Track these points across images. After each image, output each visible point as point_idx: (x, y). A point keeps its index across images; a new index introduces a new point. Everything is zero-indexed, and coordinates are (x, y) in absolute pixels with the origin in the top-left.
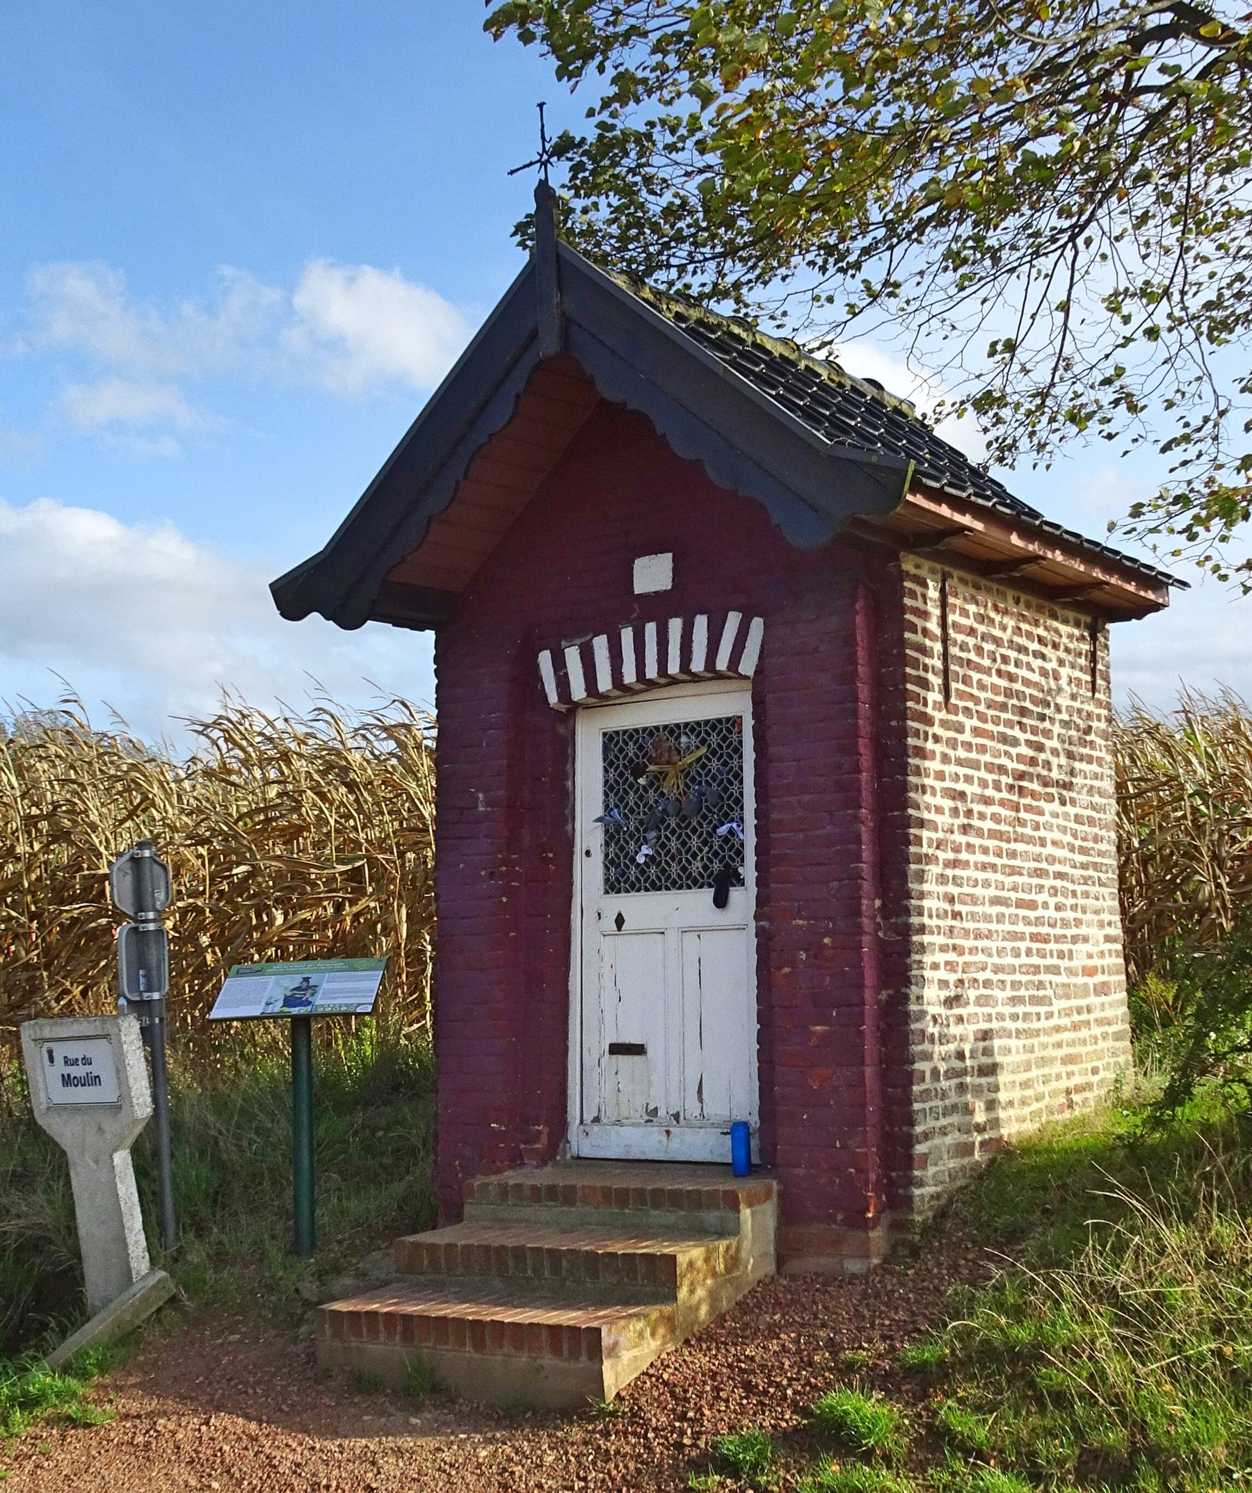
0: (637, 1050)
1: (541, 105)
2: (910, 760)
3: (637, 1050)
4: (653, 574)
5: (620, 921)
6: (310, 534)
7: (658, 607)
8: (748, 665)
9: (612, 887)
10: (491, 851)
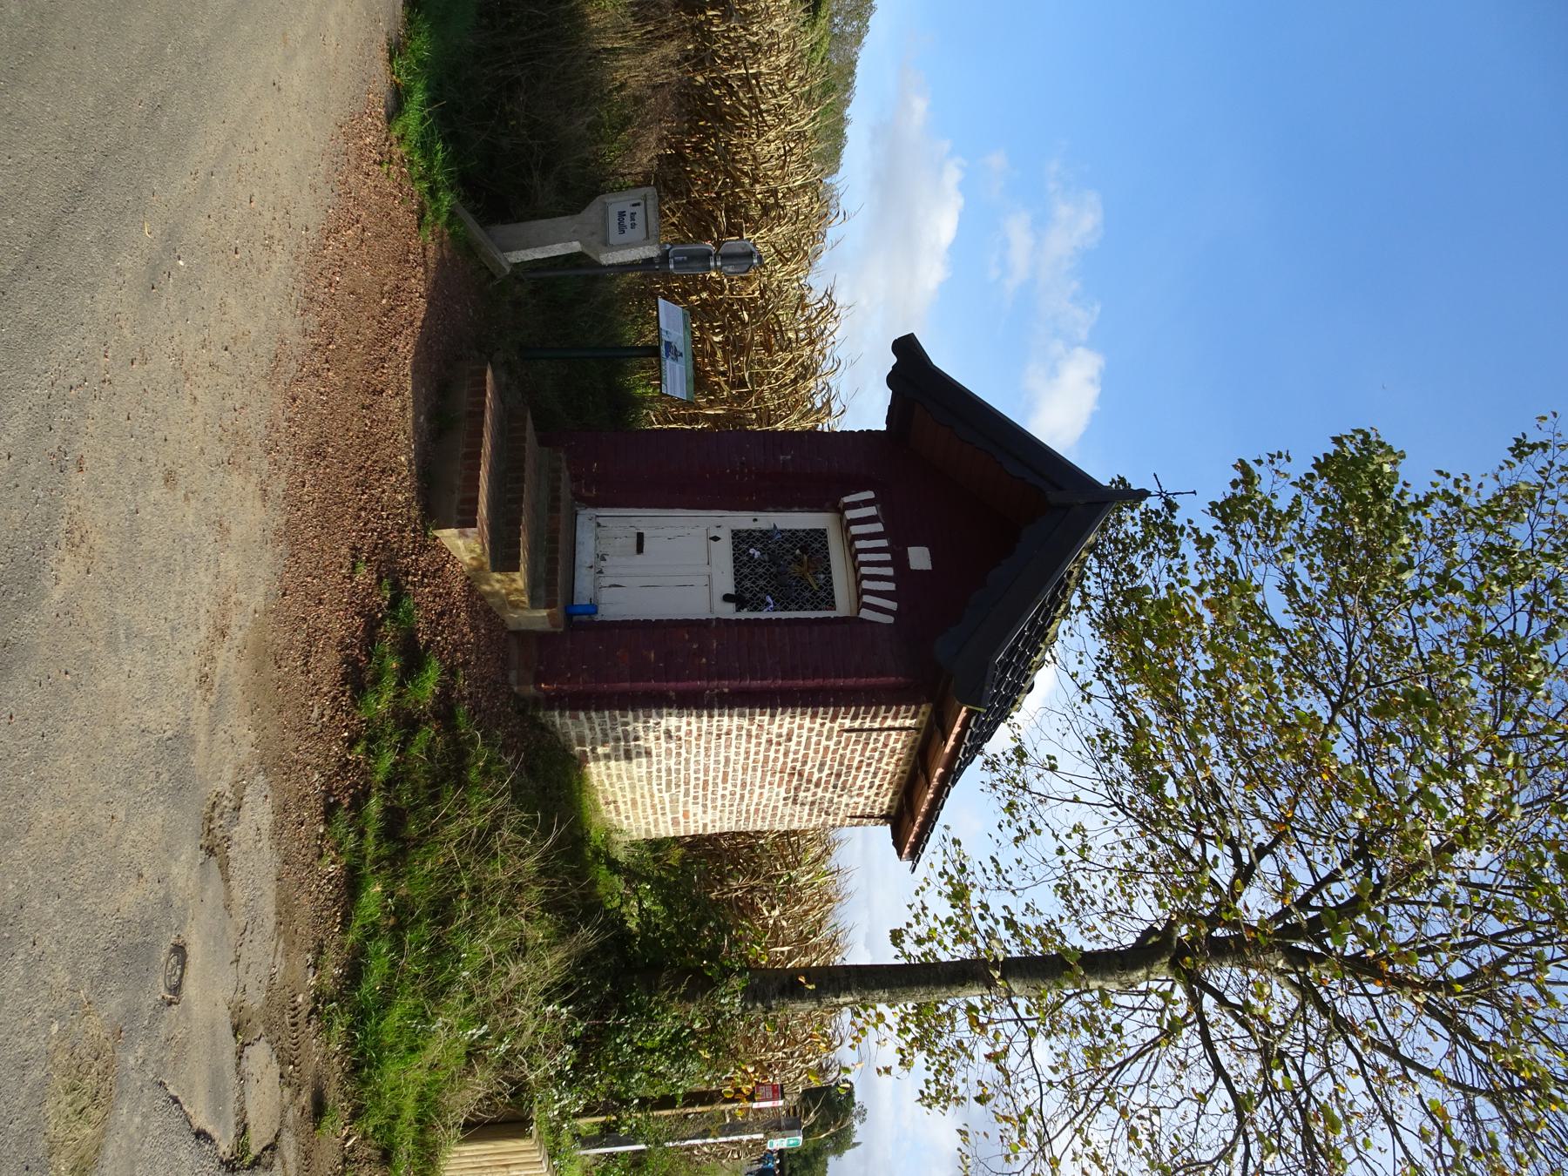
3: (640, 550)
4: (919, 558)
5: (716, 539)
7: (900, 561)
8: (865, 614)
9: (736, 534)
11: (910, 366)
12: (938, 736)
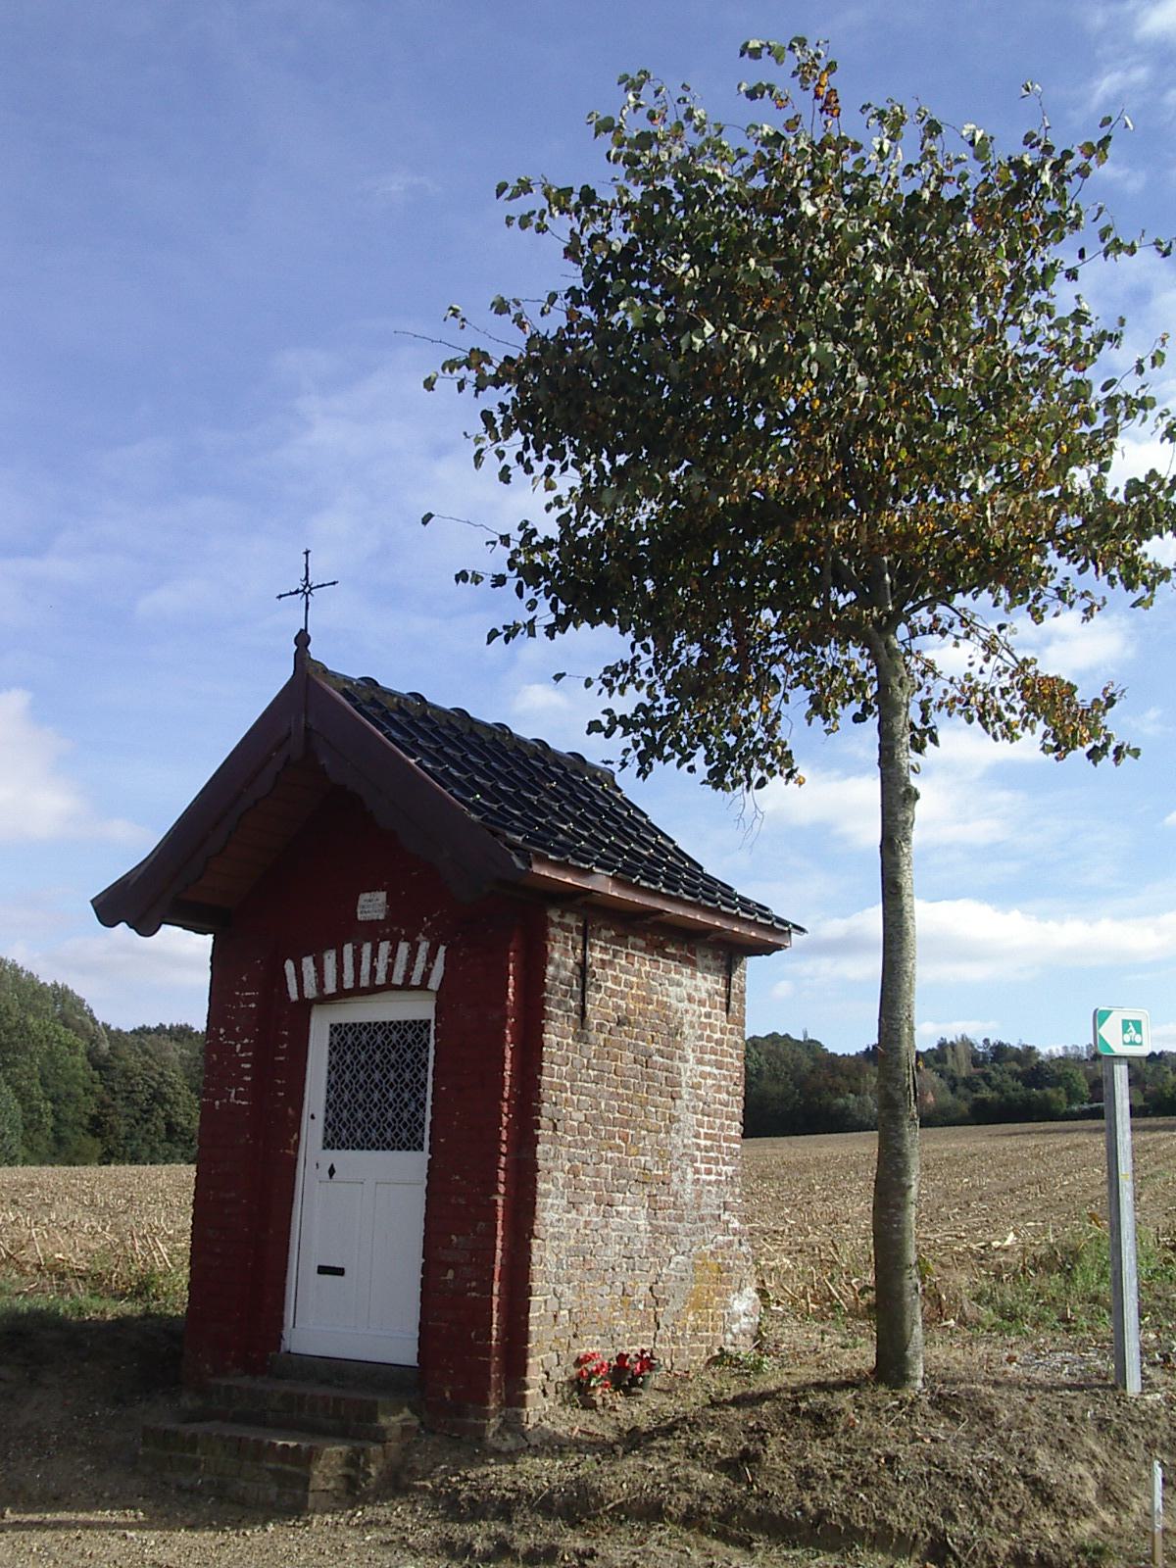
0: (340, 1272)
1: (280, 597)
2: (544, 1064)
3: (340, 1272)
4: (372, 906)
5: (332, 1171)
6: (133, 840)
7: (373, 932)
8: (434, 984)
9: (328, 1145)
10: (233, 1115)
11: (134, 903)
12: (661, 918)
